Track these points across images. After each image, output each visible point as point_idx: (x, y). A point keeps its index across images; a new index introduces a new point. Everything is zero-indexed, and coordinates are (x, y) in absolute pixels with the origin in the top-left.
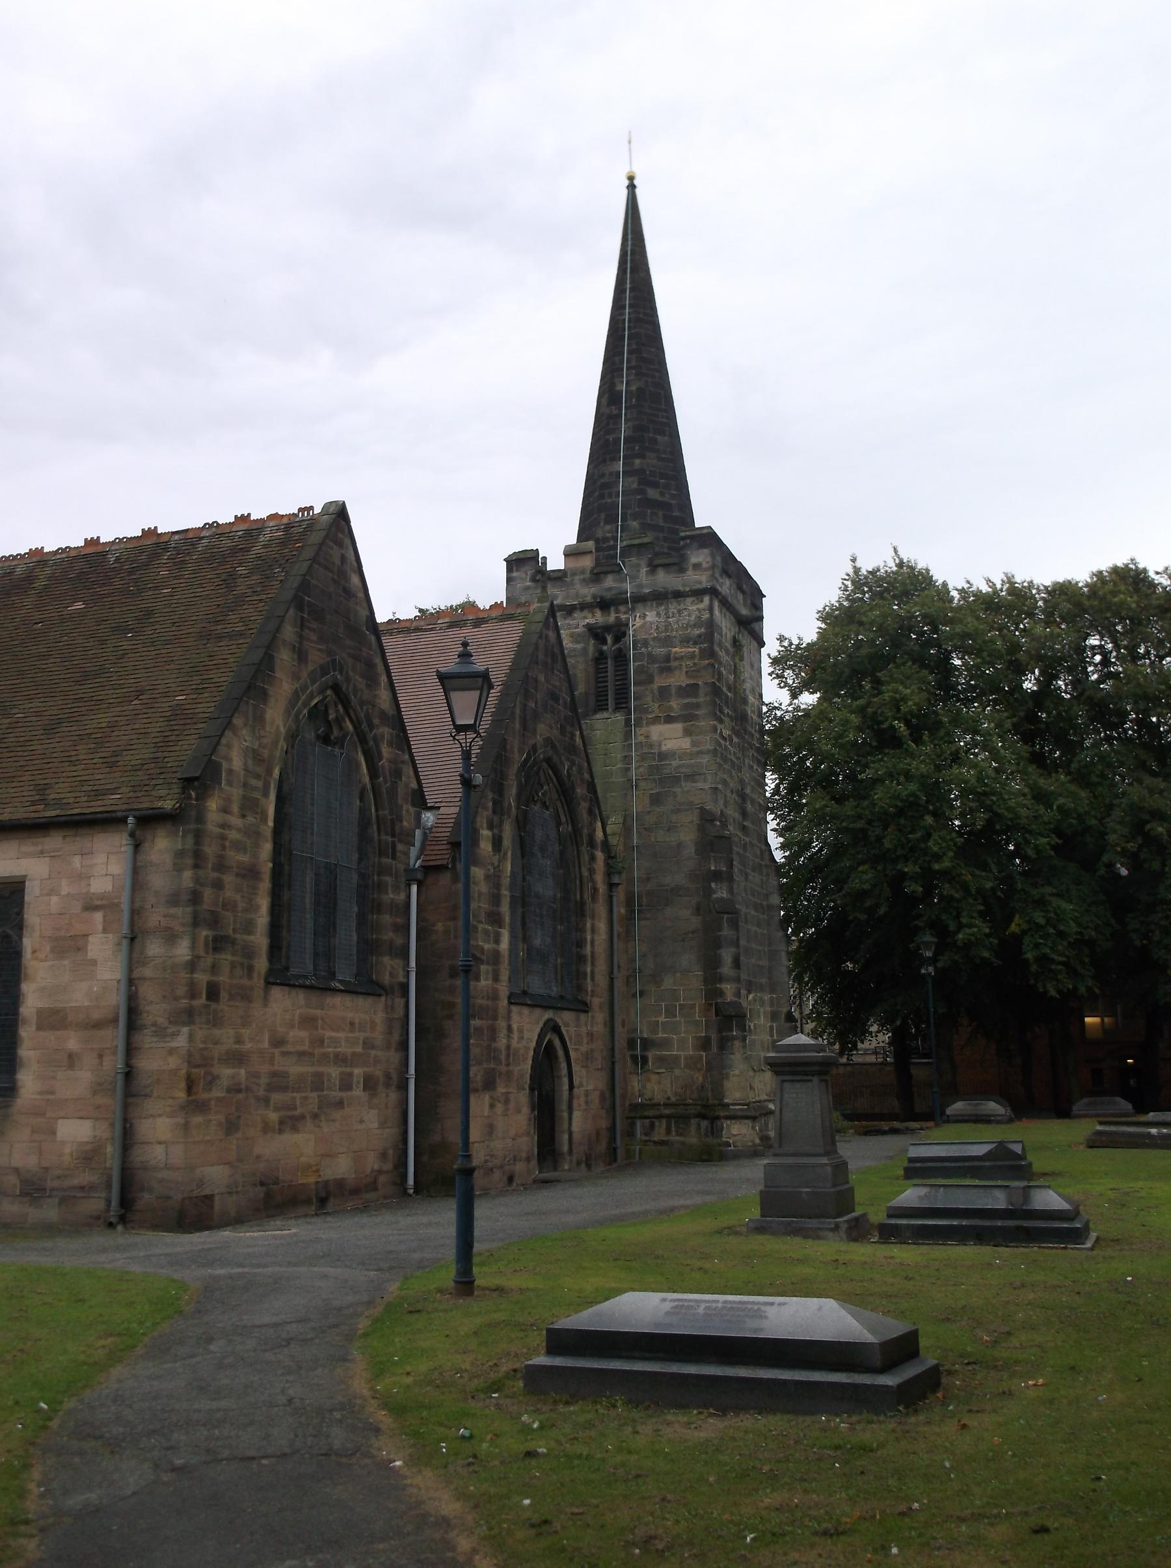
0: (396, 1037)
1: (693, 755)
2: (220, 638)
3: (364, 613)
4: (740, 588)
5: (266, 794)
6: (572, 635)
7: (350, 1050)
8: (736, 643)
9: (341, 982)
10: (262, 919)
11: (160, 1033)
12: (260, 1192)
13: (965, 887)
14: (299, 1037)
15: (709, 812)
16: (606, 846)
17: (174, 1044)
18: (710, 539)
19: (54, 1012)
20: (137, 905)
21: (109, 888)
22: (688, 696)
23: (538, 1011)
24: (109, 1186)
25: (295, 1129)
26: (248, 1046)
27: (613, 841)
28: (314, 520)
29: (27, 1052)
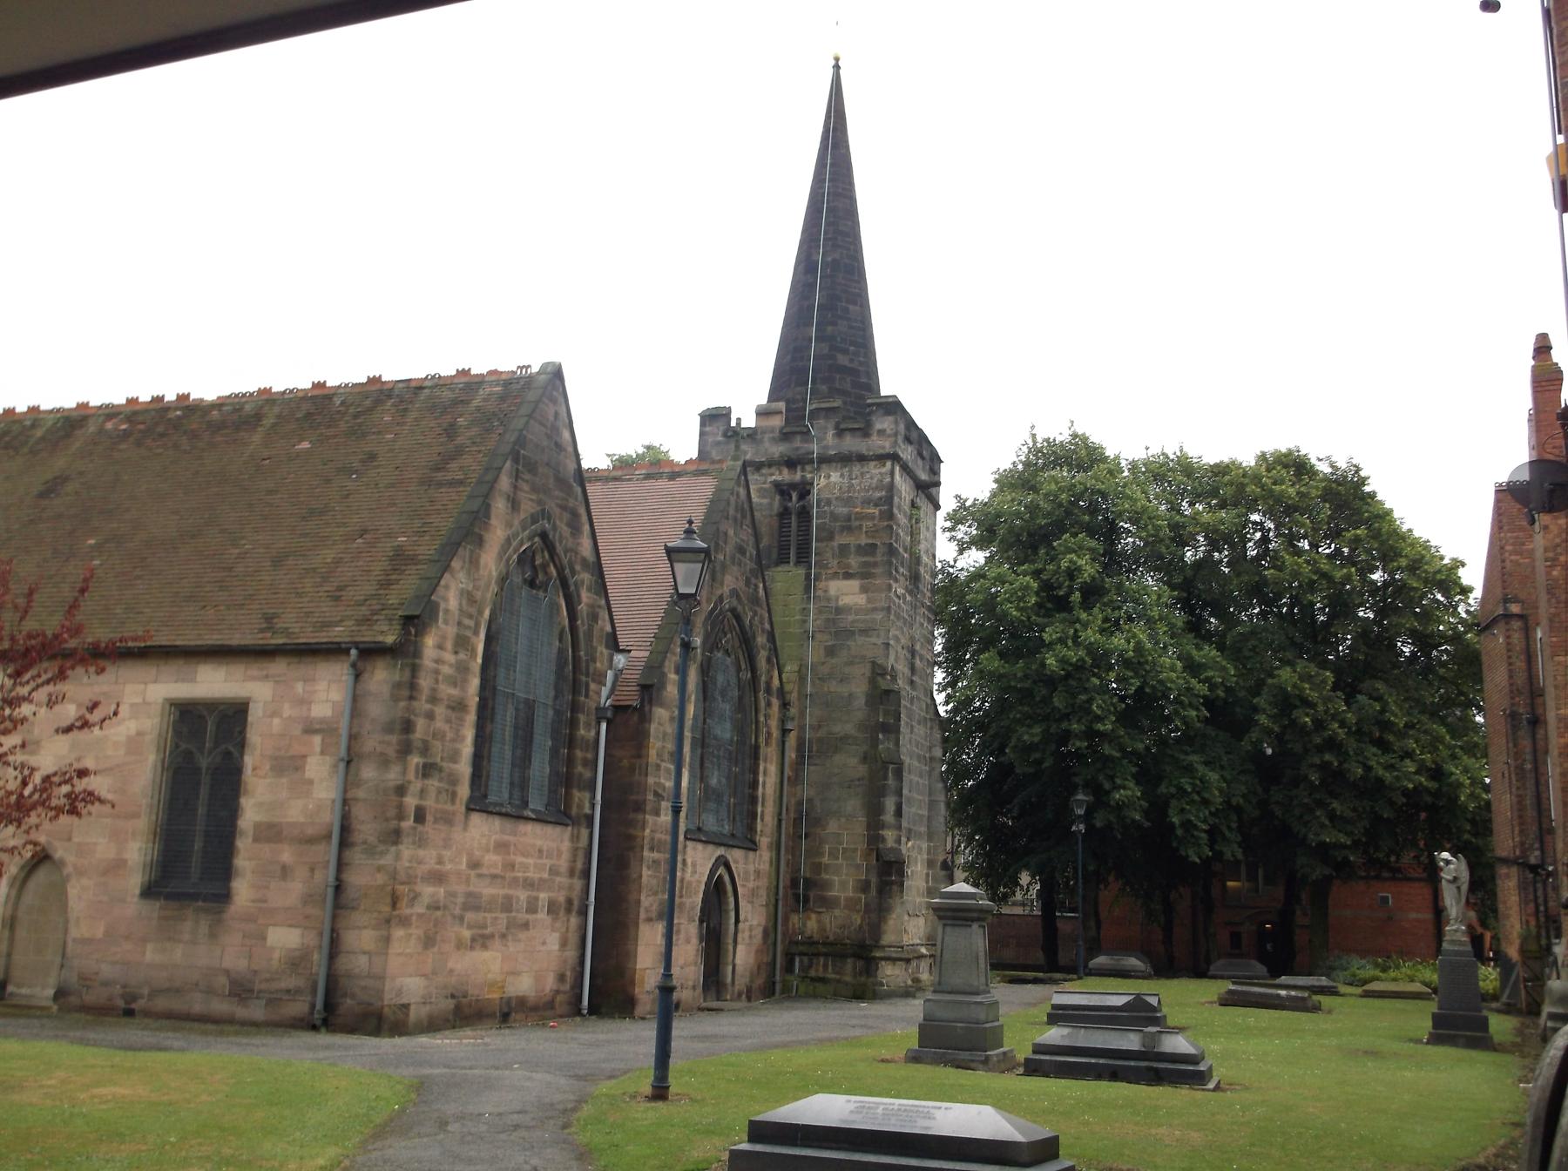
0: (579, 865)
3: (572, 466)
4: (920, 455)
5: (476, 633)
6: (759, 490)
7: (537, 876)
8: (913, 505)
9: (533, 811)
10: (467, 749)
11: (370, 851)
13: (1122, 749)
14: (493, 860)
15: (880, 666)
16: (781, 693)
17: (382, 862)
18: (894, 407)
19: (270, 826)
20: (355, 730)
21: (329, 713)
22: (866, 554)
23: (711, 847)
24: (314, 991)
25: (484, 947)
26: (449, 867)
27: (788, 688)
28: (531, 378)
29: (242, 861)
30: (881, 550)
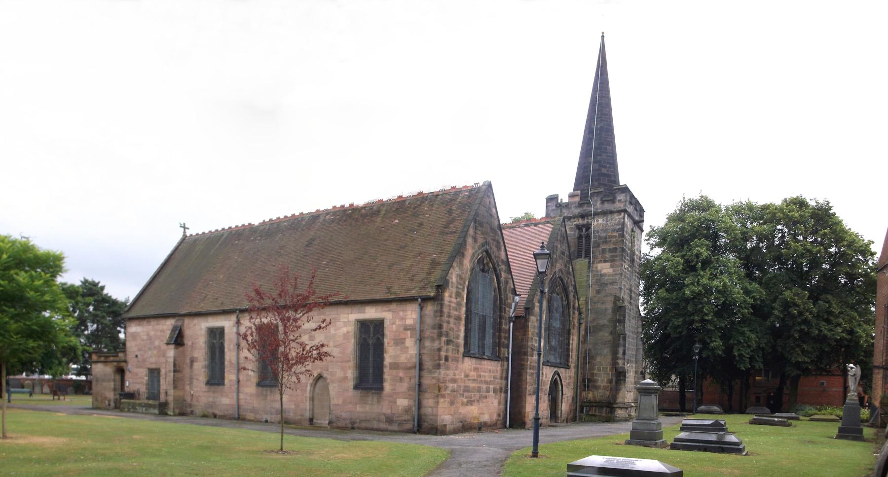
0: (504, 375)
1: (613, 275)
2: (447, 234)
8: (632, 230)
10: (462, 334)
12: (461, 424)
13: (715, 326)
14: (473, 374)
16: (579, 309)
18: (625, 190)
19: (395, 364)
24: (414, 420)
25: (471, 405)
28: (479, 188)
29: (386, 376)
30: (619, 250)
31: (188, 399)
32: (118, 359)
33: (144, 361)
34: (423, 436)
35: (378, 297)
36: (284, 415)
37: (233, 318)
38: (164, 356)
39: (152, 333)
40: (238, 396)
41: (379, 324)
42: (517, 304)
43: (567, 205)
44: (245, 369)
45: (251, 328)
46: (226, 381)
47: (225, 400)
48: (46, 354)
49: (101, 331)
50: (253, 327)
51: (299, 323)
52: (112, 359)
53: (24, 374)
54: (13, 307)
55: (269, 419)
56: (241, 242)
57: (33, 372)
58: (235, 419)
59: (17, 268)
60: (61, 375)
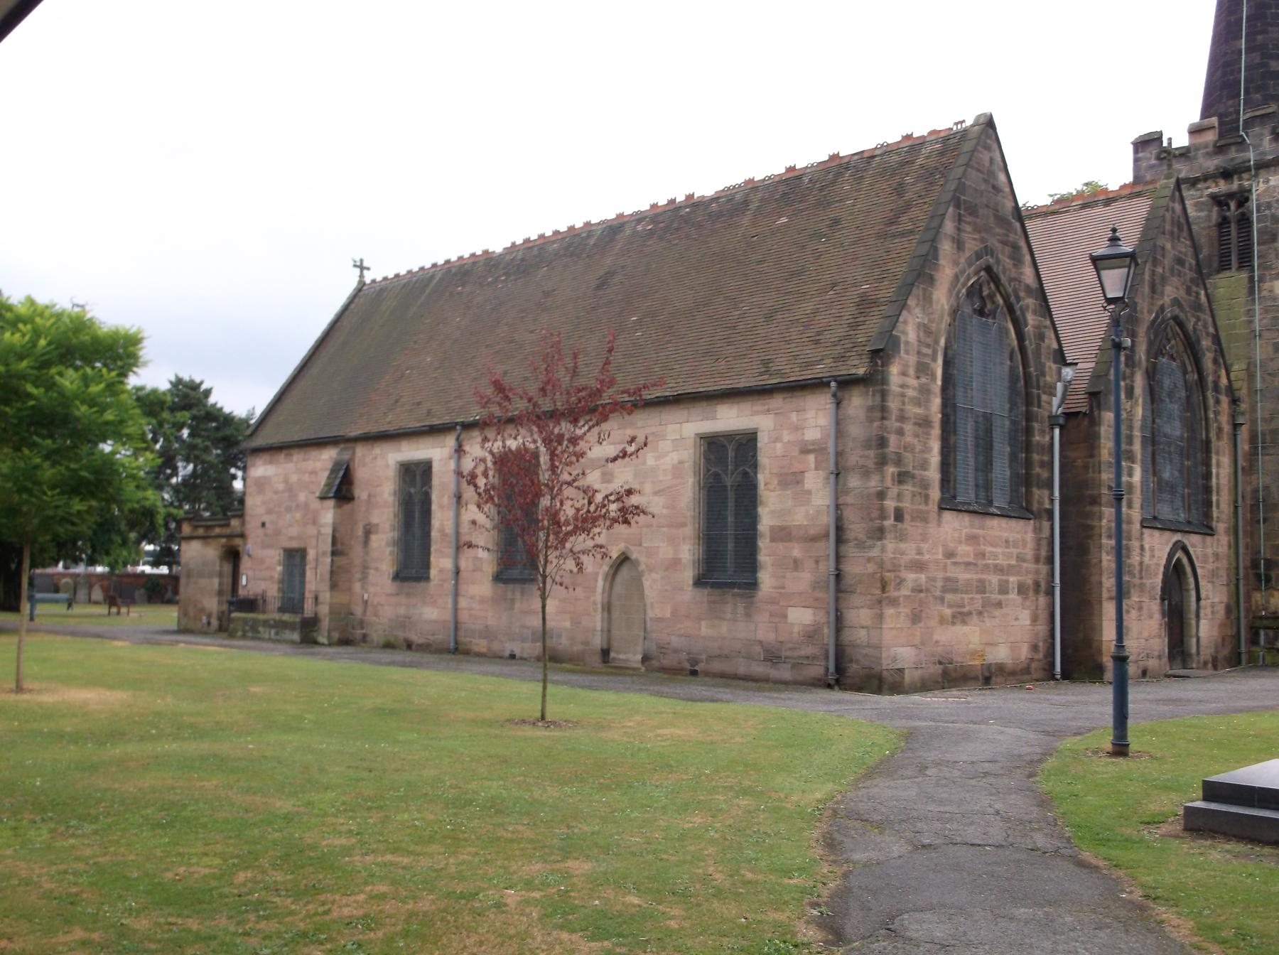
0: (1043, 553)
2: (894, 236)
10: (935, 458)
12: (939, 668)
14: (965, 551)
16: (1230, 390)
19: (782, 528)
24: (827, 658)
25: (964, 622)
29: (764, 557)
31: (358, 610)
32: (227, 531)
33: (277, 533)
34: (848, 696)
35: (743, 383)
36: (548, 644)
37: (450, 441)
38: (315, 522)
39: (294, 478)
40: (456, 603)
41: (746, 443)
42: (1067, 385)
43: (1184, 153)
44: (470, 545)
45: (483, 460)
46: (433, 572)
47: (431, 613)
48: (100, 525)
49: (201, 476)
50: (489, 458)
51: (582, 445)
52: (217, 531)
53: (61, 564)
54: (51, 436)
55: (517, 652)
56: (468, 289)
57: (76, 561)
58: (448, 651)
59: (61, 363)
60: (125, 565)
